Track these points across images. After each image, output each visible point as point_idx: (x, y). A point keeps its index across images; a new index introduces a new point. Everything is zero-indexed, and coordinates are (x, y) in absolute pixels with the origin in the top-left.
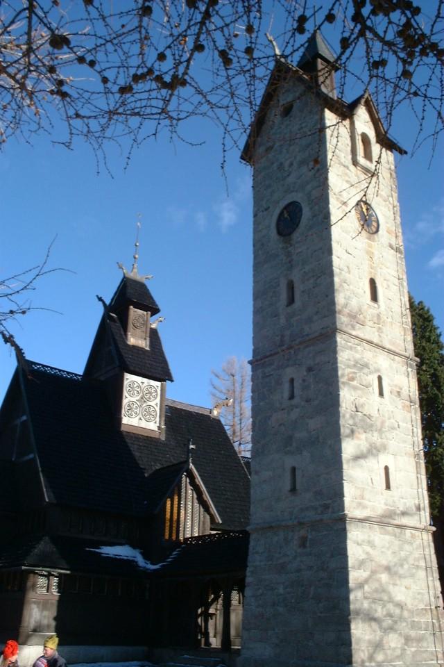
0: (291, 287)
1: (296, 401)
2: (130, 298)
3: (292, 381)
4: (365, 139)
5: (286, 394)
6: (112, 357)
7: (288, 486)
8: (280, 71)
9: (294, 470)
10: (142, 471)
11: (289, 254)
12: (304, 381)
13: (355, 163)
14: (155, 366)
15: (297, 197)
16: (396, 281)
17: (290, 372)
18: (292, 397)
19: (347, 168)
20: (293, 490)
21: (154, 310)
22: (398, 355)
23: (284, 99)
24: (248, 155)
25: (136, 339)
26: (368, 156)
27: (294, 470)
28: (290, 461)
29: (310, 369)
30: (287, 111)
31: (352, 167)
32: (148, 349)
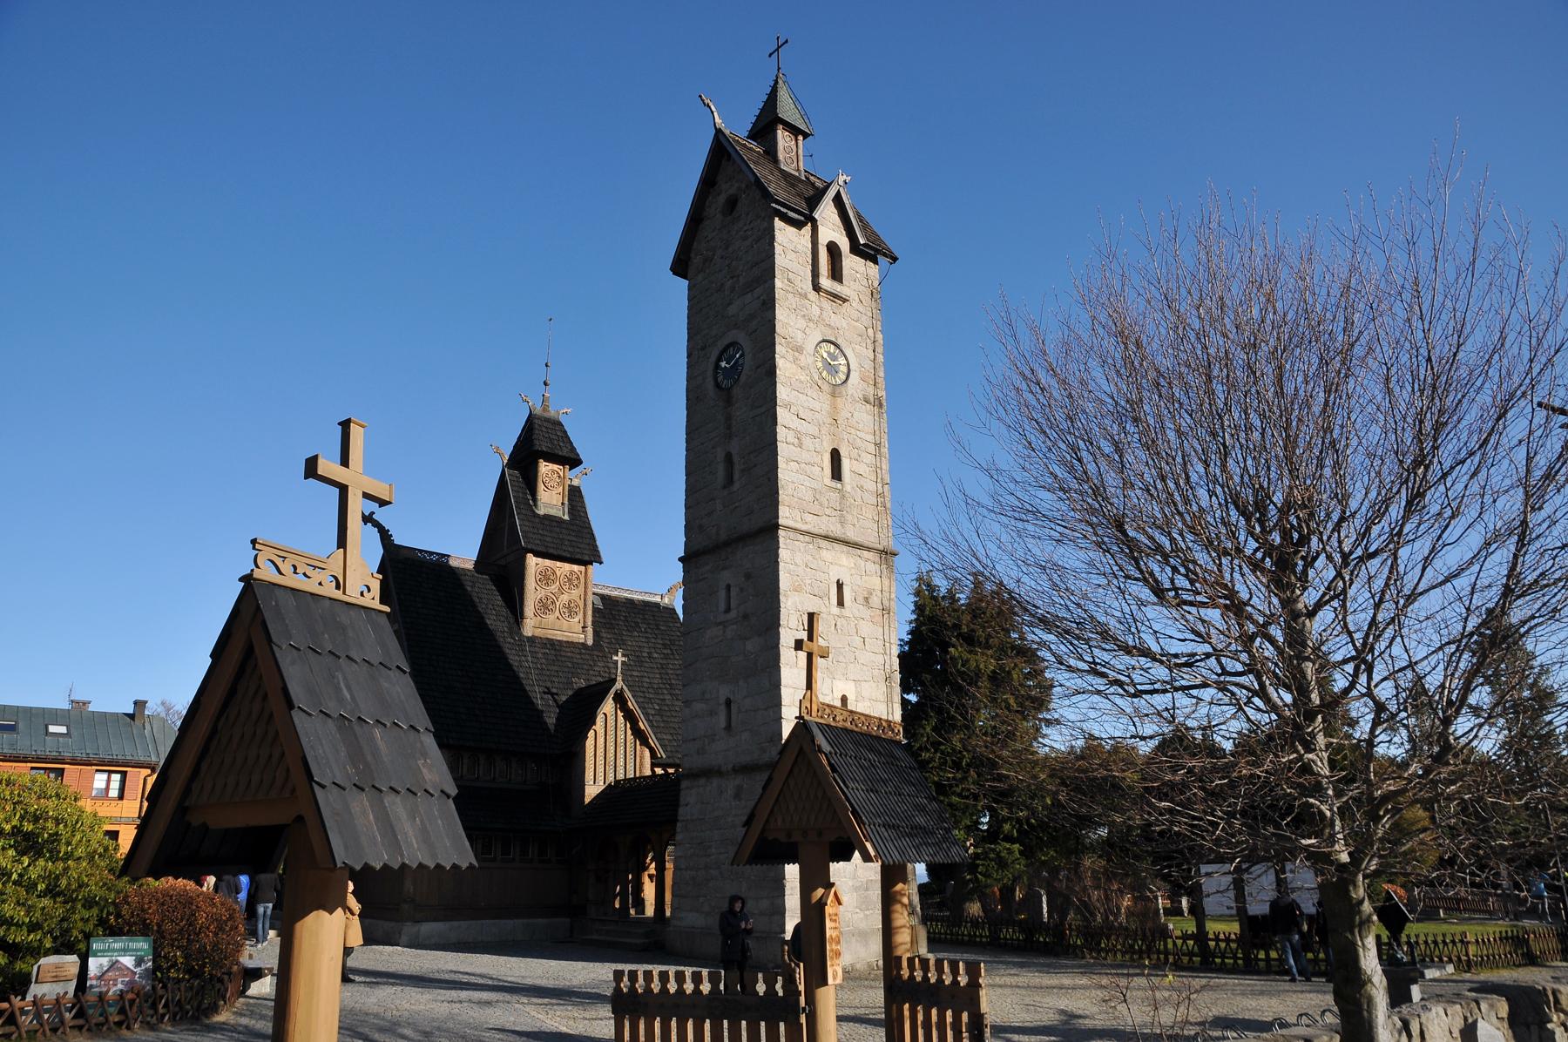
0: (729, 459)
1: (733, 614)
2: (540, 444)
3: (728, 587)
4: (833, 249)
5: (722, 606)
6: (512, 533)
7: (723, 724)
8: (721, 149)
9: (728, 703)
10: (584, 645)
11: (728, 418)
12: (742, 590)
13: (817, 288)
14: (574, 541)
15: (740, 337)
16: (872, 448)
17: (726, 577)
18: (728, 610)
19: (805, 296)
20: (728, 727)
21: (573, 461)
22: (869, 549)
23: (726, 189)
24: (680, 266)
25: (550, 500)
26: (836, 274)
27: (728, 703)
28: (724, 692)
29: (748, 576)
30: (732, 204)
31: (813, 295)
32: (566, 517)
